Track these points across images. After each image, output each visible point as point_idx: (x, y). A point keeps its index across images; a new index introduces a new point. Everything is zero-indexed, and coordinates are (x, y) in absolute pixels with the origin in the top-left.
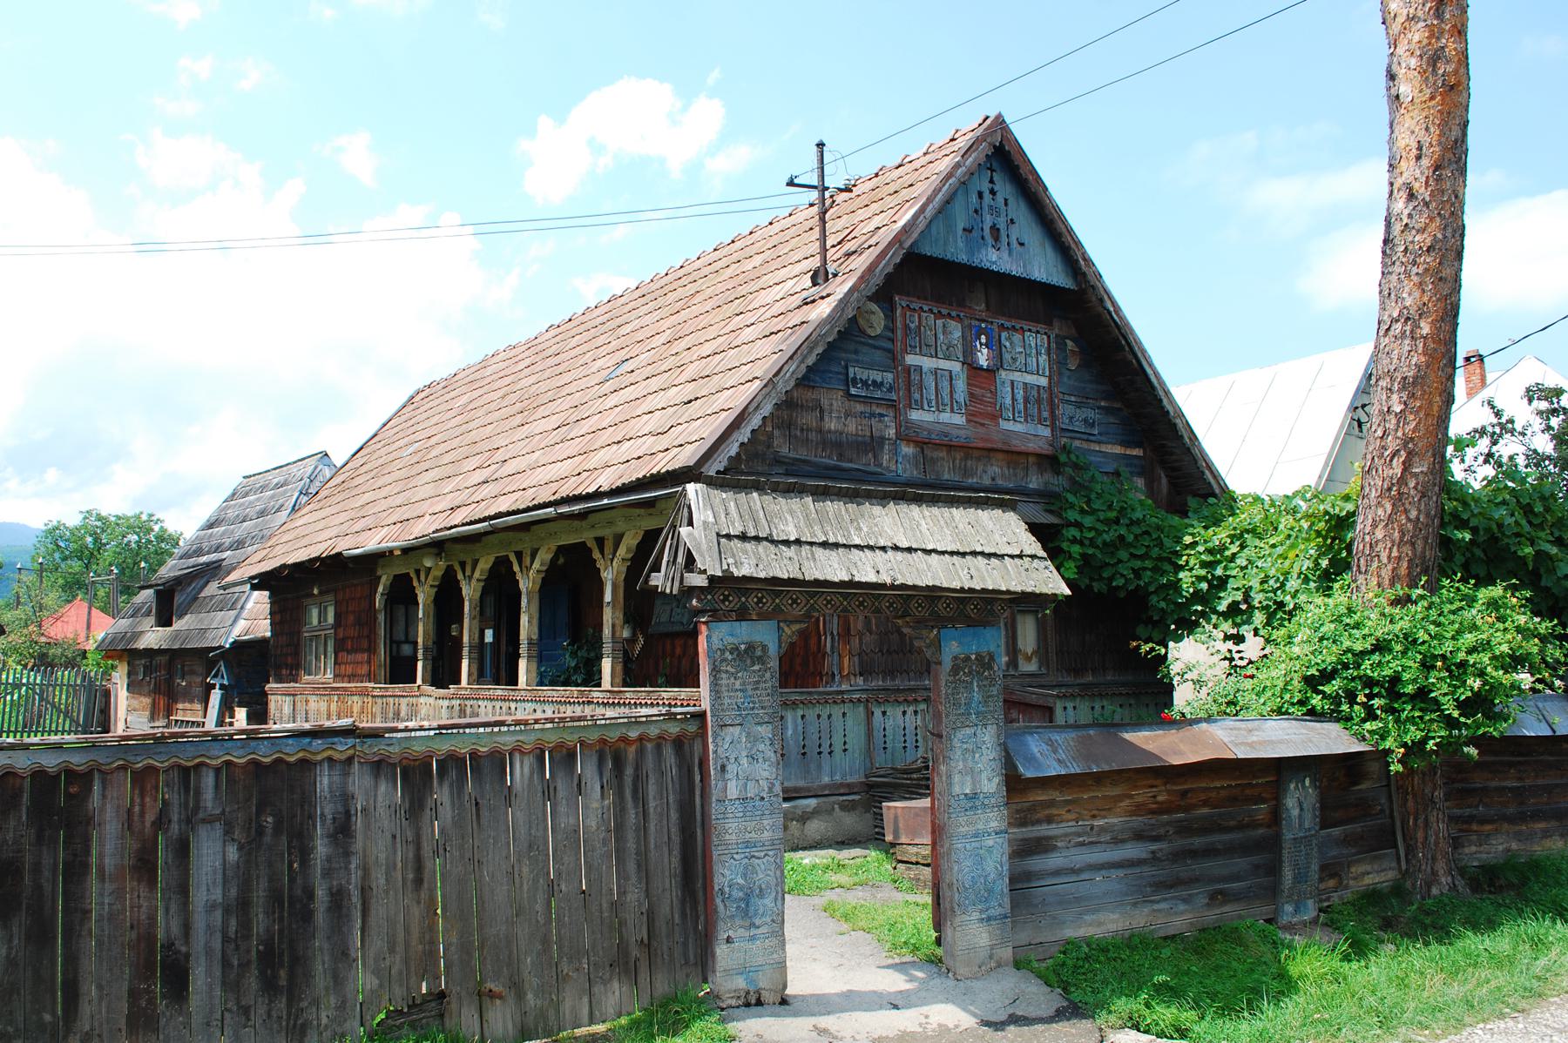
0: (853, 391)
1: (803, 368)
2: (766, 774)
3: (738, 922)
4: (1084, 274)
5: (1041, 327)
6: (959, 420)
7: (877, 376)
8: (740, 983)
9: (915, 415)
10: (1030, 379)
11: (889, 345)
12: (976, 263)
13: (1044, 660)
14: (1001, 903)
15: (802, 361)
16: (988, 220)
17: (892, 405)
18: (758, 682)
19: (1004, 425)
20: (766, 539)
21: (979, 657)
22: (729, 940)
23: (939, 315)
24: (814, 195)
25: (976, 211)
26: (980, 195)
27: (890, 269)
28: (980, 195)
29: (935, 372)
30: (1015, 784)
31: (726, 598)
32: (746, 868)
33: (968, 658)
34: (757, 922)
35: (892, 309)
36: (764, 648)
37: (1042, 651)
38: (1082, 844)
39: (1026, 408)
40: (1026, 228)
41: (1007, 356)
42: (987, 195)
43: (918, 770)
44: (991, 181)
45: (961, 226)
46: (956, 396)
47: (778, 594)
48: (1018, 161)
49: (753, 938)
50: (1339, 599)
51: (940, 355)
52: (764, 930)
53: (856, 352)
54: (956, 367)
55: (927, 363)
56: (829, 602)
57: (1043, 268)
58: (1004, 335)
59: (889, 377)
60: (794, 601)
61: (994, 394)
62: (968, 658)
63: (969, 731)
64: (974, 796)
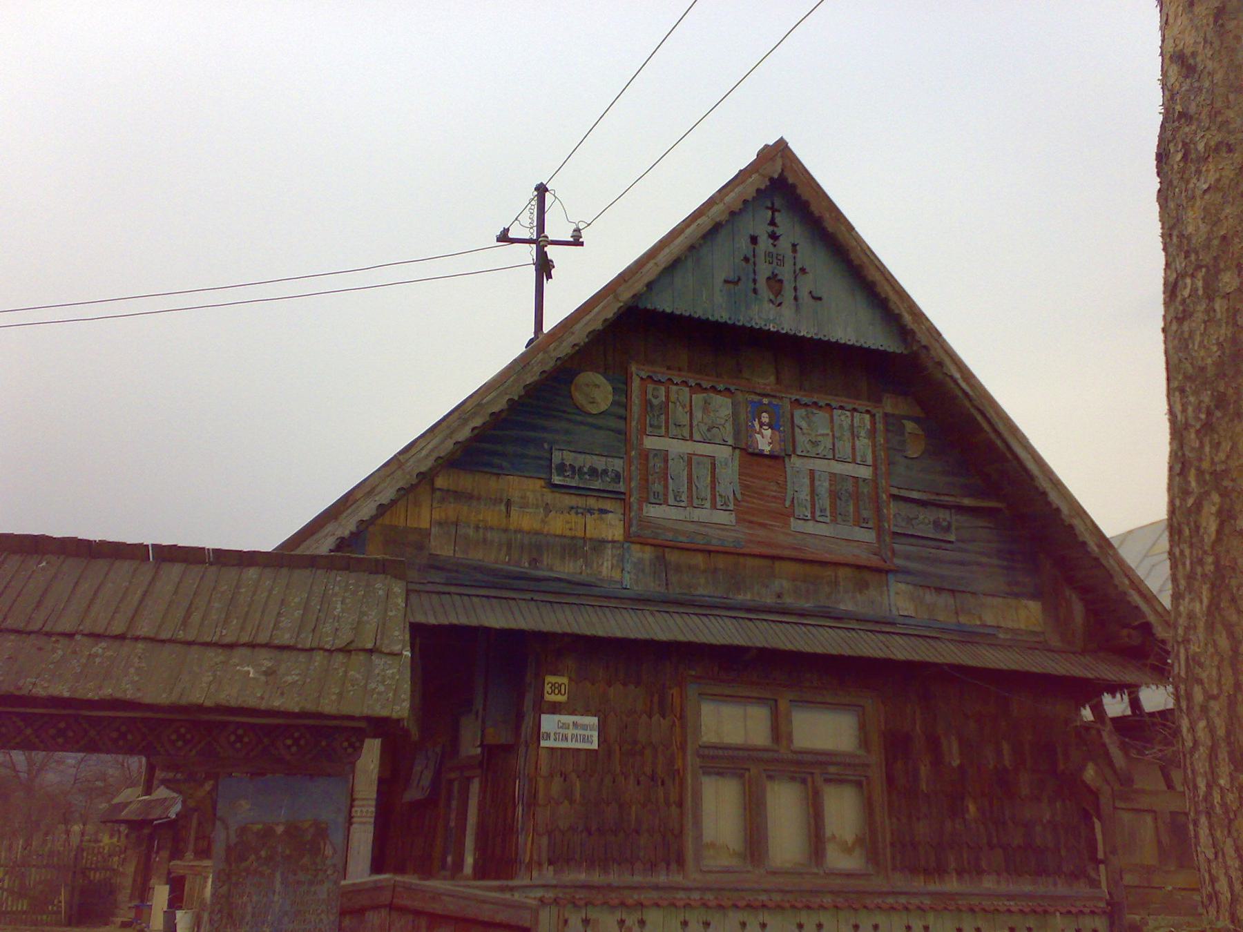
0: (557, 480)
1: (449, 445)
4: (912, 332)
5: (862, 405)
6: (723, 517)
7: (600, 463)
9: (653, 511)
10: (838, 468)
11: (620, 425)
12: (742, 320)
13: (873, 855)
15: (450, 436)
16: (764, 270)
17: (619, 496)
19: (795, 525)
20: (266, 646)
21: (293, 831)
23: (700, 388)
24: (530, 252)
25: (746, 259)
26: (754, 240)
27: (598, 325)
28: (754, 240)
29: (689, 459)
33: (268, 832)
35: (627, 381)
37: (869, 843)
39: (833, 505)
40: (821, 273)
41: (801, 440)
42: (764, 243)
44: (772, 223)
45: (720, 276)
46: (720, 489)
48: (804, 193)
51: (697, 436)
53: (567, 432)
54: (723, 453)
55: (676, 447)
57: (874, 337)
58: (799, 413)
59: (617, 464)
61: (783, 487)
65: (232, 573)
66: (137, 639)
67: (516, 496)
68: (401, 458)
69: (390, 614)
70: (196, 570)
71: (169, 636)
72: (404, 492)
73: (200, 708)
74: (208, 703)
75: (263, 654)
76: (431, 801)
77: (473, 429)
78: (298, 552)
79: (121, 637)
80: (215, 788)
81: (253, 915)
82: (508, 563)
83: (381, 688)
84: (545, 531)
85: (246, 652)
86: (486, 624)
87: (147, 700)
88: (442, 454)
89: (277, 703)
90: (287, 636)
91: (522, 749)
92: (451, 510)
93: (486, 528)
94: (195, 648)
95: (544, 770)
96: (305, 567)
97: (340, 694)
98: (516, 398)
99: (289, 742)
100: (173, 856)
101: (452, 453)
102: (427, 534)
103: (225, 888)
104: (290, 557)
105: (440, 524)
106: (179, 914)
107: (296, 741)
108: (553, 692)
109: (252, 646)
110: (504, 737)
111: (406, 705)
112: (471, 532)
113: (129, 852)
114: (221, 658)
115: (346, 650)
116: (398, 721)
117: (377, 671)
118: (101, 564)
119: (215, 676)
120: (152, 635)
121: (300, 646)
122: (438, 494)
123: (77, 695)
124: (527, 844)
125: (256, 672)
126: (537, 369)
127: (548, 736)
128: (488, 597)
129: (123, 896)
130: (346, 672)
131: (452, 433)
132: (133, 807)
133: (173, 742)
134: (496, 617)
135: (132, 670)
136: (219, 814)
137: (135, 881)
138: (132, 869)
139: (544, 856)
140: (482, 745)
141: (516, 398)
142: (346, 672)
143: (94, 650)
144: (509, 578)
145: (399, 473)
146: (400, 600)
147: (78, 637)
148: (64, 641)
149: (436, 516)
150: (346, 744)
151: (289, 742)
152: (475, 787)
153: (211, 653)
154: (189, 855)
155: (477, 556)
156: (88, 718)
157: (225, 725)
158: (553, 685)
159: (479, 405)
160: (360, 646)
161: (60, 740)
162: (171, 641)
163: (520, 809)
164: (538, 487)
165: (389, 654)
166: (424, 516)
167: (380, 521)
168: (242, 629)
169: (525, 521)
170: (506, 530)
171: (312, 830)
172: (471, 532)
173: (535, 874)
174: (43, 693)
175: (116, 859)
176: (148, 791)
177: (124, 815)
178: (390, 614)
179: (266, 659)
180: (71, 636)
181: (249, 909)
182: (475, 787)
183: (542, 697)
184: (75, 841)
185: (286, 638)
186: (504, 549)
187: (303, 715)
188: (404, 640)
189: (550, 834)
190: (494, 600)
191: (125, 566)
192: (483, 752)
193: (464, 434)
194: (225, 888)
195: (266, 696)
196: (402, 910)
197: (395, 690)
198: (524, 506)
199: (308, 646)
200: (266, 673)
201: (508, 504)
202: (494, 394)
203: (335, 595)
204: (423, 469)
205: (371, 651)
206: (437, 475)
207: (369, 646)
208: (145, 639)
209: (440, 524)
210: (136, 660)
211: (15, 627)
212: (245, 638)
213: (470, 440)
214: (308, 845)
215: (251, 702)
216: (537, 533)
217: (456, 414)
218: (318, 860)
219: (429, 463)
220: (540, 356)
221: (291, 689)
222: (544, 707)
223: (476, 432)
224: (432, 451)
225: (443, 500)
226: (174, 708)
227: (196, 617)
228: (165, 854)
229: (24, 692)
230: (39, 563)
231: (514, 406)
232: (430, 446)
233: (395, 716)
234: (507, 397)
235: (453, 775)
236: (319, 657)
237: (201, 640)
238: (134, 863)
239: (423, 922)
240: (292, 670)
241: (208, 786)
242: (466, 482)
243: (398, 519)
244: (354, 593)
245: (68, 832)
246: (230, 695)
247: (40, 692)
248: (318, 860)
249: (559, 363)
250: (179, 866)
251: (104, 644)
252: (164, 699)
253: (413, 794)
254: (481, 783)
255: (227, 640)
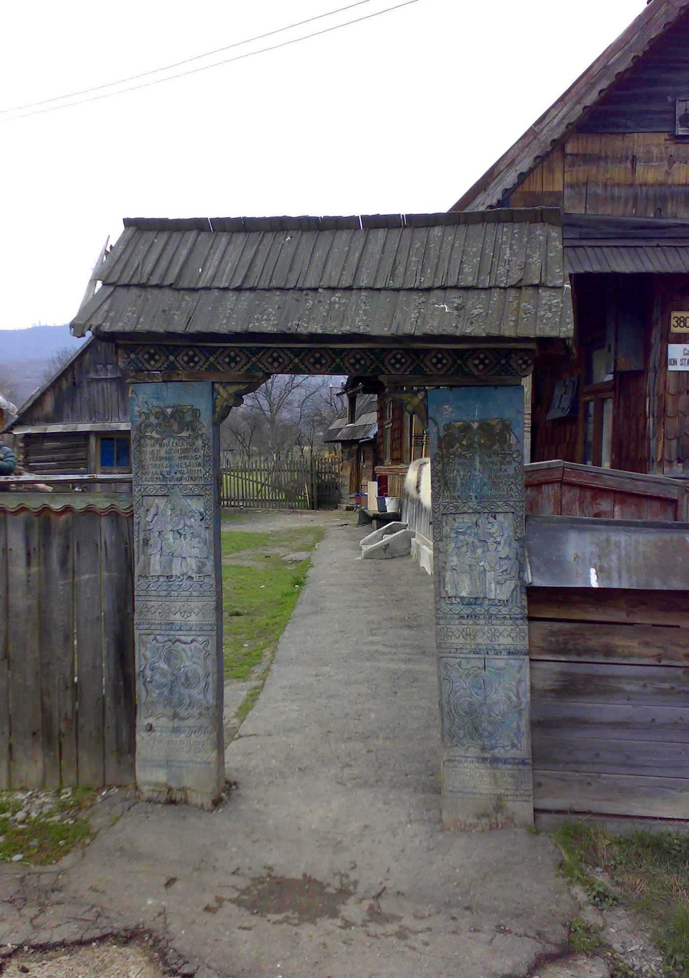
1: (579, 109)
2: (195, 552)
3: (160, 709)
8: (161, 776)
14: (515, 743)
18: (186, 450)
21: (485, 427)
22: (150, 728)
30: (541, 600)
31: (152, 357)
32: (169, 652)
33: (467, 428)
34: (183, 712)
36: (195, 412)
38: (661, 692)
43: (467, 359)
47: (212, 351)
49: (176, 730)
50: (342, 945)
52: (190, 722)
56: (275, 360)
60: (233, 359)
62: (467, 428)
63: (467, 519)
64: (474, 601)
65: (422, 233)
66: (360, 289)
67: (640, 151)
68: (536, 129)
69: (551, 255)
70: (395, 234)
71: (383, 286)
72: (540, 160)
73: (412, 338)
74: (418, 333)
75: (453, 295)
76: (570, 419)
77: (601, 91)
78: (466, 211)
79: (349, 289)
80: (426, 396)
81: (462, 484)
82: (635, 215)
83: (550, 315)
84: (670, 181)
85: (438, 293)
86: (618, 270)
87: (375, 333)
88: (572, 121)
89: (468, 331)
90: (470, 279)
91: (651, 375)
92: (581, 173)
93: (613, 185)
94: (402, 293)
95: (672, 389)
96: (477, 223)
97: (516, 321)
98: (641, 55)
99: (477, 362)
100: (375, 464)
101: (580, 119)
102: (558, 196)
103: (440, 465)
104: (460, 216)
105: (572, 186)
106: (387, 500)
107: (482, 362)
108: (679, 325)
109: (444, 288)
110: (634, 365)
111: (571, 326)
112: (599, 191)
113: (345, 462)
114: (423, 299)
115: (517, 287)
116: (563, 340)
117: (544, 302)
118: (326, 236)
119: (420, 313)
120: (371, 285)
121: (481, 286)
122: (569, 158)
123: (327, 332)
124: (657, 448)
125: (450, 308)
126: (661, 22)
127: (675, 362)
128: (616, 247)
129: (345, 490)
130: (519, 304)
131: (580, 99)
132: (344, 431)
133: (393, 365)
134: (625, 264)
135: (361, 312)
136: (431, 414)
137: (351, 482)
138: (349, 473)
139: (674, 458)
140: (615, 373)
141: (641, 55)
142: (519, 304)
143: (333, 299)
144: (636, 228)
145: (536, 142)
146: (558, 243)
147: (321, 290)
148: (311, 293)
149: (568, 178)
150: (520, 362)
151: (477, 362)
152: (609, 406)
153: (415, 296)
154: (388, 461)
155: (607, 211)
156: (333, 350)
157: (428, 351)
158: (679, 319)
159: (605, 67)
160: (529, 282)
161: (318, 366)
162: (385, 289)
163: (650, 422)
164: (662, 142)
165: (552, 287)
166: (557, 181)
167: (520, 189)
168: (435, 276)
169: (649, 174)
170: (631, 185)
171: (499, 427)
172: (599, 191)
173: (666, 469)
174: (304, 331)
175: (337, 466)
176: (352, 420)
177: (339, 436)
178: (551, 255)
179: (456, 298)
180: (315, 290)
181: (459, 480)
182: (609, 406)
183: (669, 328)
184: (307, 456)
185: (470, 281)
186: (631, 203)
187: (489, 339)
188: (564, 275)
189: (678, 439)
190: (622, 250)
191: (344, 235)
192: (615, 377)
193: (593, 97)
194: (440, 465)
195: (460, 326)
196: (571, 485)
197: (561, 316)
198: (649, 160)
199: (487, 285)
200: (457, 309)
201: (634, 160)
202: (620, 54)
203: (505, 243)
204: (556, 137)
205: (537, 286)
206: (566, 142)
207: (536, 282)
208: (366, 289)
209: (572, 186)
210: (362, 305)
211: (278, 286)
212: (438, 284)
213: (596, 104)
214: (495, 436)
215: (449, 331)
216: (661, 185)
217: (584, 79)
218: (506, 447)
219: (562, 129)
220: (663, 8)
221: (477, 319)
222: (669, 338)
223: (603, 94)
224: (564, 118)
225: (573, 164)
226: (396, 339)
227: (401, 269)
228: (370, 463)
229: (293, 331)
230: (286, 238)
231: (639, 63)
232: (561, 115)
233: (562, 335)
234: (633, 55)
235: (588, 398)
236: (496, 294)
237: (406, 287)
238: (349, 468)
239: (588, 495)
240: (476, 305)
241: (421, 396)
242: (593, 144)
243: (535, 186)
244: (519, 240)
245: (302, 450)
246: (432, 327)
247: (302, 330)
248: (506, 447)
249: (683, 12)
250: (380, 470)
251: (339, 295)
252: (385, 331)
253: (555, 413)
254: (614, 403)
255: (425, 286)
